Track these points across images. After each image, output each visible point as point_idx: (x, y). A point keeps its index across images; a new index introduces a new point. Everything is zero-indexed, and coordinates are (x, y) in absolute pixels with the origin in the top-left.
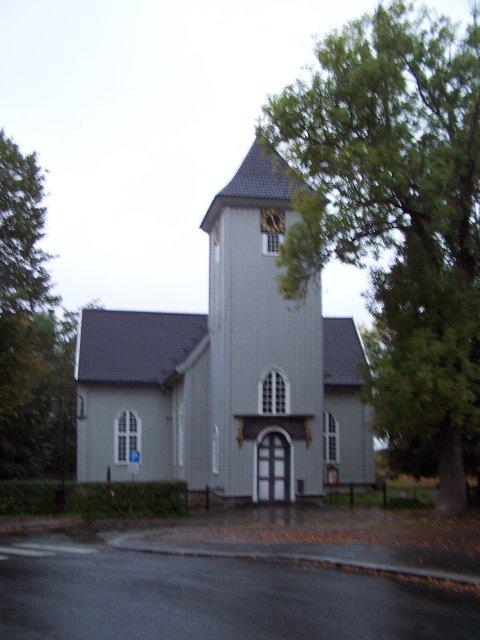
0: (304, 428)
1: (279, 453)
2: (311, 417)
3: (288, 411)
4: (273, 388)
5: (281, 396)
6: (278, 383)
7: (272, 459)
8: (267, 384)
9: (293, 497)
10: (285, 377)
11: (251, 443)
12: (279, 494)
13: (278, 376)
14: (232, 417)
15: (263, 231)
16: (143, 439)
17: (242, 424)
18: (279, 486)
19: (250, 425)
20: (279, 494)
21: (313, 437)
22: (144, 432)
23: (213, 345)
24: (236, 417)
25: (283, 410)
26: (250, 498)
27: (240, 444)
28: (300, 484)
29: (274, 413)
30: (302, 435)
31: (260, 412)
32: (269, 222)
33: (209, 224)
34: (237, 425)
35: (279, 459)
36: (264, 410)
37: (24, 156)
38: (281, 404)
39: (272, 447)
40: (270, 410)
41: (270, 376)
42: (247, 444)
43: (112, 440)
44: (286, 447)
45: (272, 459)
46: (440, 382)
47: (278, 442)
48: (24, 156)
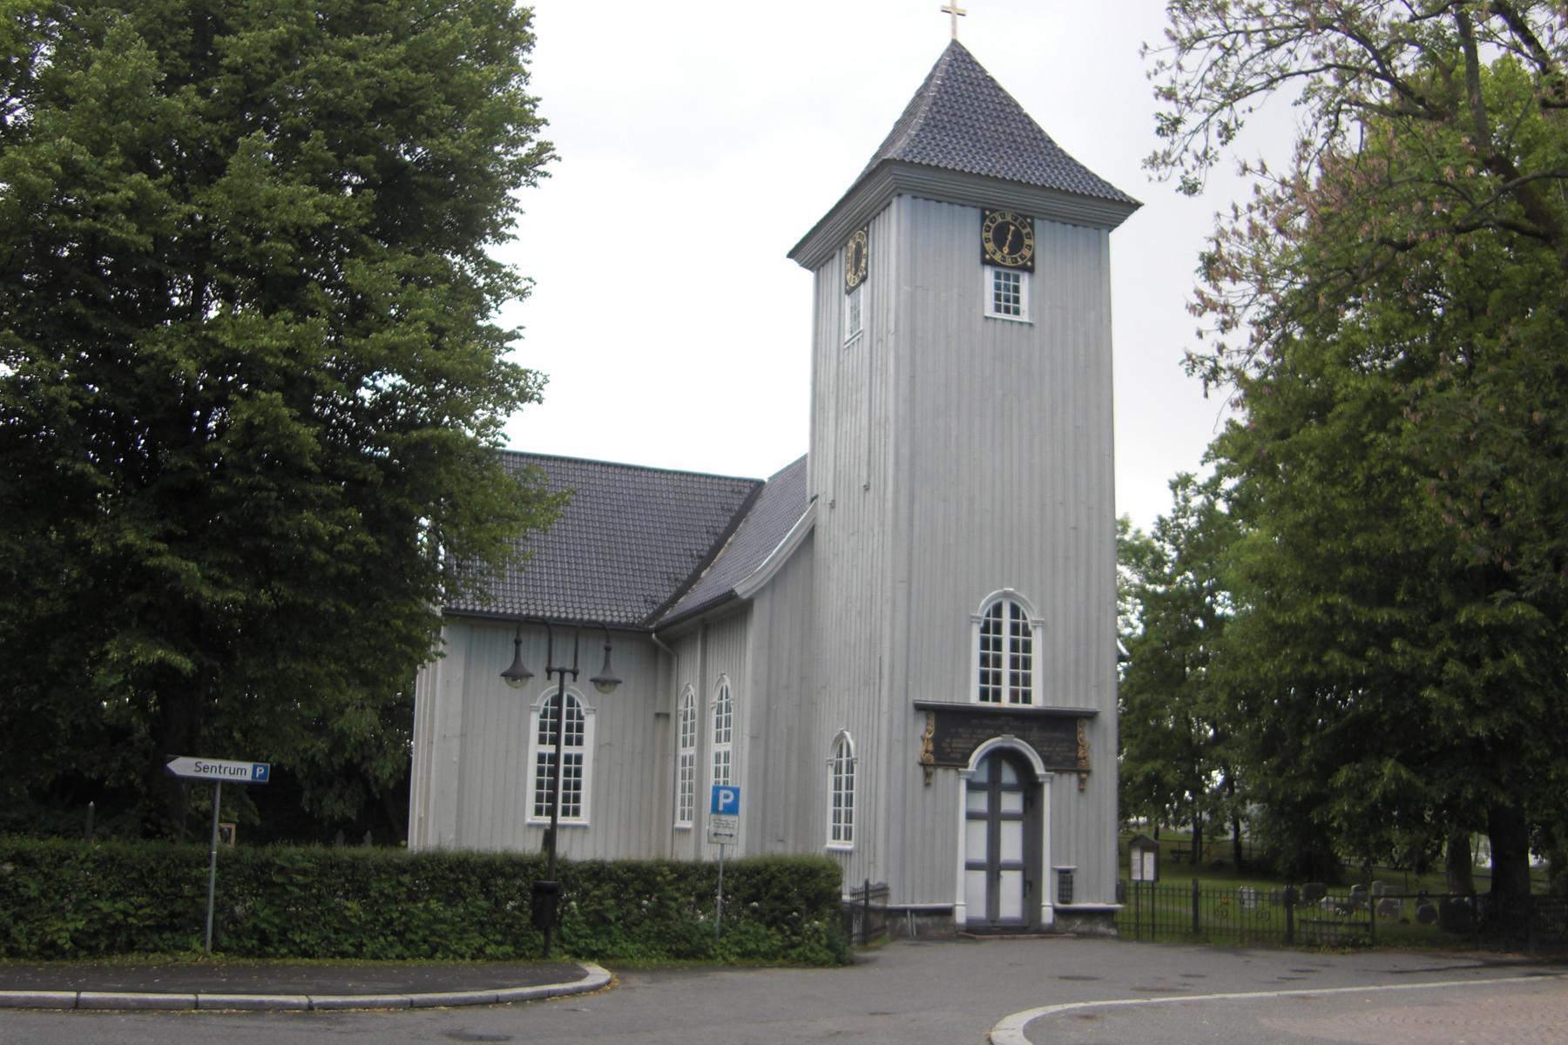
0: (1075, 744)
1: (1012, 803)
2: (1091, 716)
3: (1038, 701)
4: (1003, 633)
5: (1022, 663)
6: (1015, 629)
7: (994, 818)
8: (991, 628)
9: (1047, 916)
10: (1032, 616)
11: (952, 772)
12: (1011, 906)
13: (1015, 611)
14: (911, 709)
15: (985, 262)
16: (597, 760)
17: (932, 728)
18: (1011, 883)
19: (951, 730)
20: (1011, 906)
21: (1095, 767)
22: (599, 747)
23: (820, 534)
24: (920, 708)
25: (1027, 697)
26: (948, 912)
27: (928, 775)
28: (1065, 880)
29: (1005, 702)
30: (1071, 762)
31: (974, 700)
32: (999, 242)
33: (832, 244)
34: (922, 729)
35: (1011, 817)
36: (984, 695)
37: (1119, 516)
38: (1021, 680)
39: (994, 788)
40: (997, 696)
41: (997, 610)
42: (943, 777)
43: (477, 762)
44: (1031, 789)
45: (994, 818)
46: (1224, 244)
47: (1008, 776)
48: (1119, 516)
